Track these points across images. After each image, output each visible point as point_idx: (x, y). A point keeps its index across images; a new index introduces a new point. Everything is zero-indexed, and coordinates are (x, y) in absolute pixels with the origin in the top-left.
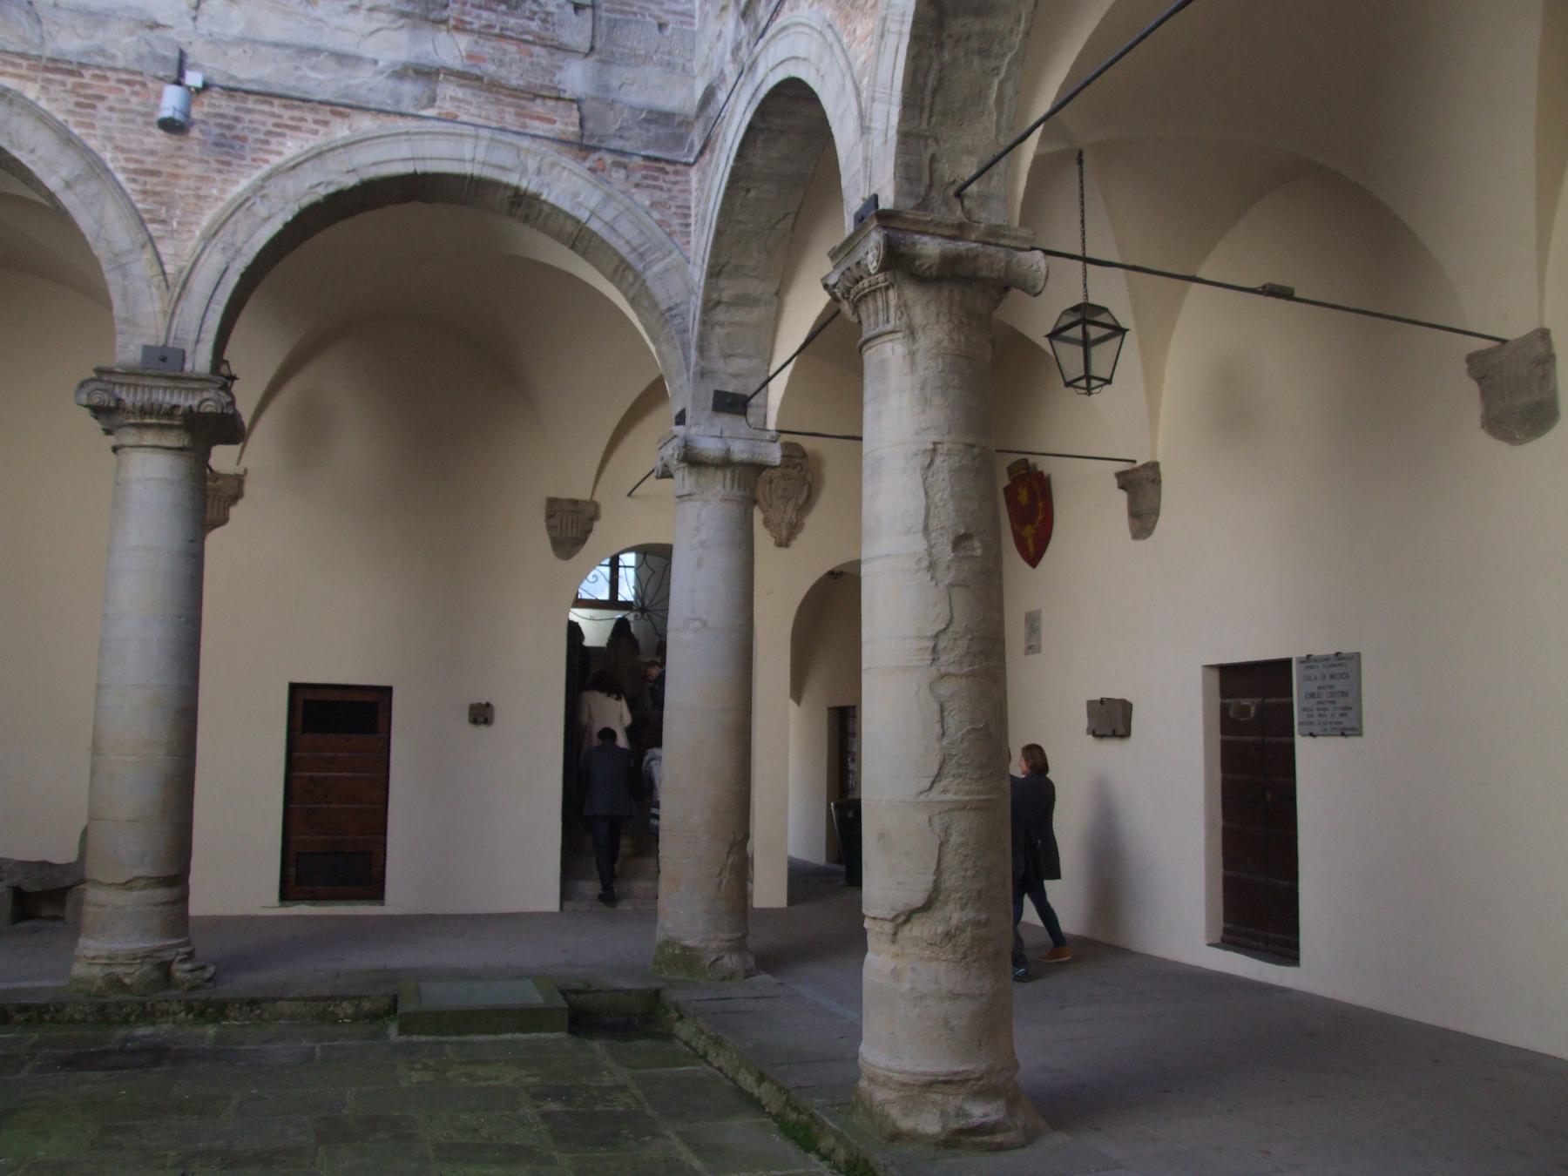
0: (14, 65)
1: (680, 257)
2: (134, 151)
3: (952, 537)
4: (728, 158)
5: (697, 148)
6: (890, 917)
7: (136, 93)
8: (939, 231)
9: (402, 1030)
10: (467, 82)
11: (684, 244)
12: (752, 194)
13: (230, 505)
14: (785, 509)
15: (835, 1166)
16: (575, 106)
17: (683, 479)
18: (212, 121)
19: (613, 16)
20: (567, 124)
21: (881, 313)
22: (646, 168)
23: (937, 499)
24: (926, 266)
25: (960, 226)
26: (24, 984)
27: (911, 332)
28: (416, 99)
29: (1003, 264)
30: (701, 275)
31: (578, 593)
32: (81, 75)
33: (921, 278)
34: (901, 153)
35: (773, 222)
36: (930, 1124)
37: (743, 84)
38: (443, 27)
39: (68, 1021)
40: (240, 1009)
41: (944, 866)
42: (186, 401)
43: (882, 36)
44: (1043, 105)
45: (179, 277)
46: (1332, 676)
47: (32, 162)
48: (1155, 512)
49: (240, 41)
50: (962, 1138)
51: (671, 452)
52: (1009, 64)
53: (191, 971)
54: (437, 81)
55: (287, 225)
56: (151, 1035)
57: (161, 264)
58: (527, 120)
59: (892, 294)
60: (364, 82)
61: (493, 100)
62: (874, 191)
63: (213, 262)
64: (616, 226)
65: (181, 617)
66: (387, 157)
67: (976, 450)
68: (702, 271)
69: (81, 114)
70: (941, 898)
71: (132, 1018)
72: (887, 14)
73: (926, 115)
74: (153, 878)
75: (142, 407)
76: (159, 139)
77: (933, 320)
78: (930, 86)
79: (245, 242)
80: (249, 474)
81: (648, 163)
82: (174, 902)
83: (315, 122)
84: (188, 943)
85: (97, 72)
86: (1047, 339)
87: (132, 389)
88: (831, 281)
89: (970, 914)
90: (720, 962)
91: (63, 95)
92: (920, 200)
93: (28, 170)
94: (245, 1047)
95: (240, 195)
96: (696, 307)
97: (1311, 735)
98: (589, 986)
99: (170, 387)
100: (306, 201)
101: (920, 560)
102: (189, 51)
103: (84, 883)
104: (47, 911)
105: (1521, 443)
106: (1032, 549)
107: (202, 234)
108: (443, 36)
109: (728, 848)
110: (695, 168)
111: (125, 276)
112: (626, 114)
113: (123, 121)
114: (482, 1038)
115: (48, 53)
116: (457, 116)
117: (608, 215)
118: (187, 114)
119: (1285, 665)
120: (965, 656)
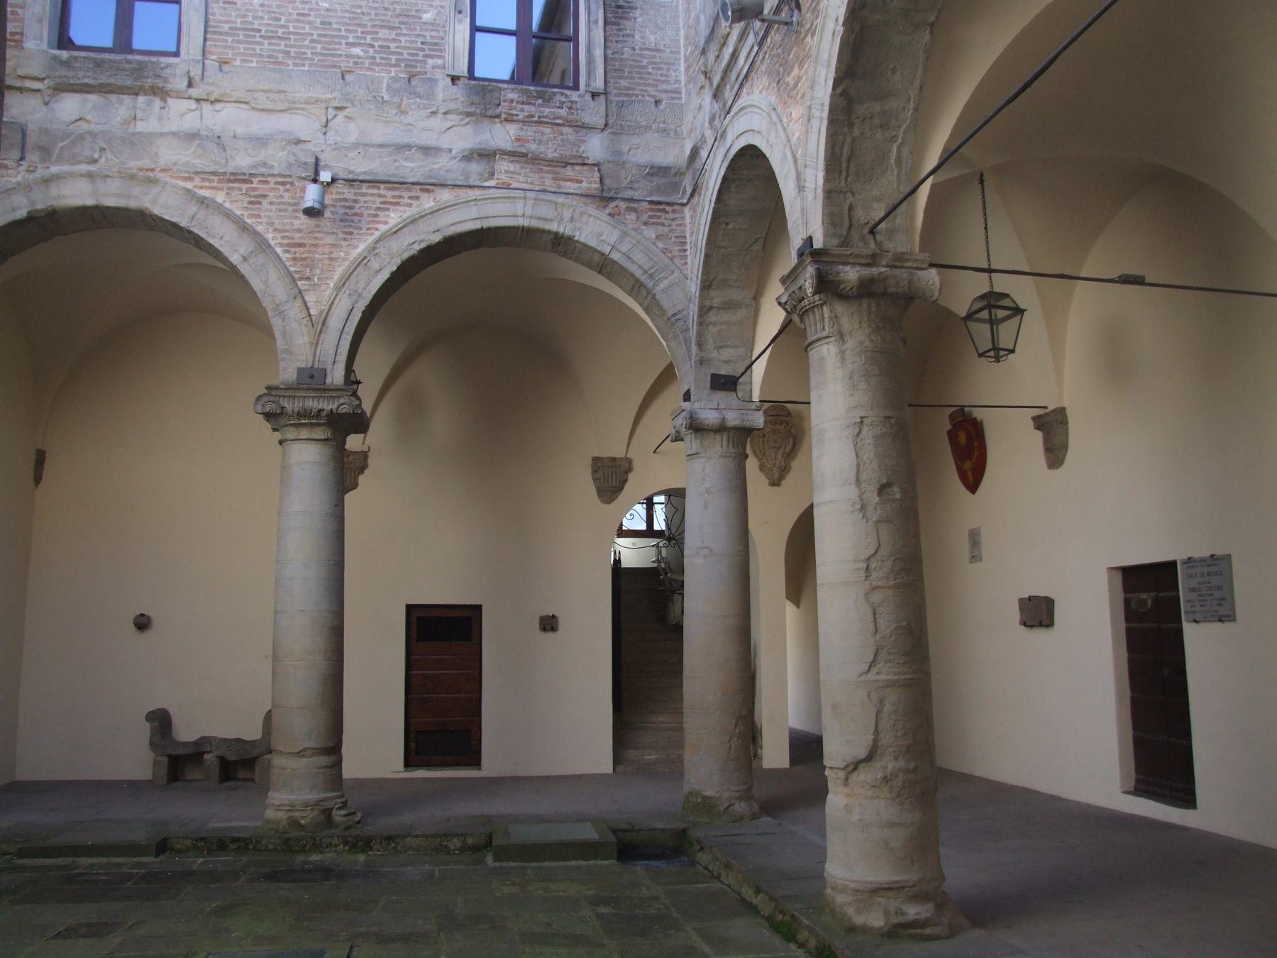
0: (209, 181)
1: (681, 275)
2: (287, 231)
3: (877, 486)
4: (710, 202)
5: (689, 192)
6: (842, 766)
7: (286, 190)
8: (858, 261)
9: (496, 859)
10: (516, 159)
11: (683, 265)
12: (731, 226)
13: (359, 474)
14: (776, 456)
15: (809, 952)
16: (596, 169)
17: (691, 441)
18: (338, 204)
19: (621, 99)
20: (590, 182)
21: (818, 323)
22: (651, 210)
23: (865, 457)
24: (848, 288)
25: (874, 256)
26: (232, 824)
27: (841, 337)
28: (481, 174)
29: (906, 282)
30: (697, 288)
31: (621, 524)
32: (252, 182)
33: (843, 297)
34: (826, 206)
35: (748, 245)
36: (876, 920)
37: (717, 148)
38: (497, 120)
39: (265, 850)
40: (381, 842)
41: (880, 728)
42: (328, 406)
43: (809, 120)
44: (932, 160)
45: (320, 317)
46: (1209, 574)
47: (221, 246)
48: (1065, 447)
49: (356, 146)
50: (900, 930)
51: (681, 421)
53: (346, 815)
54: (495, 160)
55: (393, 274)
56: (320, 860)
57: (308, 310)
58: (561, 182)
59: (825, 309)
60: (443, 166)
61: (536, 170)
62: (809, 234)
63: (343, 304)
64: (631, 256)
65: (330, 561)
67: (892, 421)
68: (697, 285)
69: (252, 209)
70: (879, 752)
71: (307, 848)
73: (844, 174)
74: (317, 749)
75: (299, 412)
76: (304, 221)
77: (856, 326)
78: (845, 155)
80: (371, 450)
81: (652, 206)
82: (332, 766)
83: (410, 198)
84: (343, 796)
85: (262, 179)
88: (783, 300)
89: (901, 763)
92: (843, 238)
93: (218, 251)
94: (386, 869)
95: (360, 255)
96: (694, 312)
97: (1195, 621)
98: (633, 827)
100: (406, 256)
102: (321, 157)
103: (270, 752)
104: (242, 774)
106: (971, 478)
107: (335, 285)
108: (497, 127)
109: (735, 722)
110: (688, 206)
111: (283, 320)
112: (634, 171)
114: (554, 864)
115: (230, 170)
117: (625, 247)
118: (322, 203)
119: (1172, 565)
120: (890, 573)
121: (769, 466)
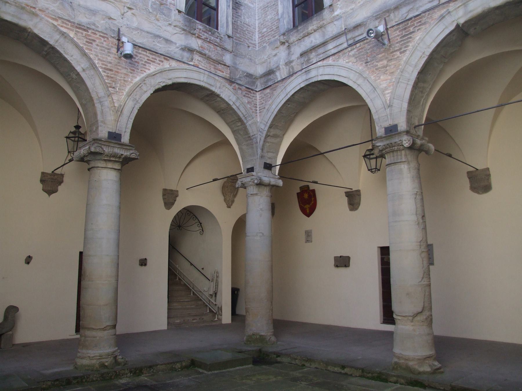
0: (66, 23)
3: (421, 217)
7: (105, 41)
20: (226, 74)
22: (246, 90)
28: (188, 58)
32: (88, 32)
38: (194, 36)
39: (92, 381)
47: (71, 60)
49: (137, 29)
52: (426, 95)
58: (217, 71)
60: (174, 50)
63: (130, 104)
66: (180, 76)
71: (113, 377)
72: (400, 77)
74: (112, 326)
79: (139, 99)
81: (247, 89)
83: (160, 61)
86: (363, 157)
87: (107, 147)
90: (270, 339)
91: (82, 37)
99: (120, 148)
101: (416, 222)
105: (481, 194)
111: (102, 106)
113: (101, 50)
116: (199, 66)
121: (228, 199)
